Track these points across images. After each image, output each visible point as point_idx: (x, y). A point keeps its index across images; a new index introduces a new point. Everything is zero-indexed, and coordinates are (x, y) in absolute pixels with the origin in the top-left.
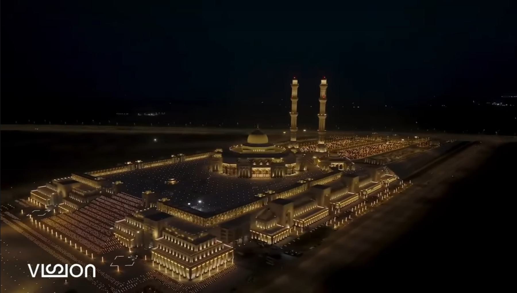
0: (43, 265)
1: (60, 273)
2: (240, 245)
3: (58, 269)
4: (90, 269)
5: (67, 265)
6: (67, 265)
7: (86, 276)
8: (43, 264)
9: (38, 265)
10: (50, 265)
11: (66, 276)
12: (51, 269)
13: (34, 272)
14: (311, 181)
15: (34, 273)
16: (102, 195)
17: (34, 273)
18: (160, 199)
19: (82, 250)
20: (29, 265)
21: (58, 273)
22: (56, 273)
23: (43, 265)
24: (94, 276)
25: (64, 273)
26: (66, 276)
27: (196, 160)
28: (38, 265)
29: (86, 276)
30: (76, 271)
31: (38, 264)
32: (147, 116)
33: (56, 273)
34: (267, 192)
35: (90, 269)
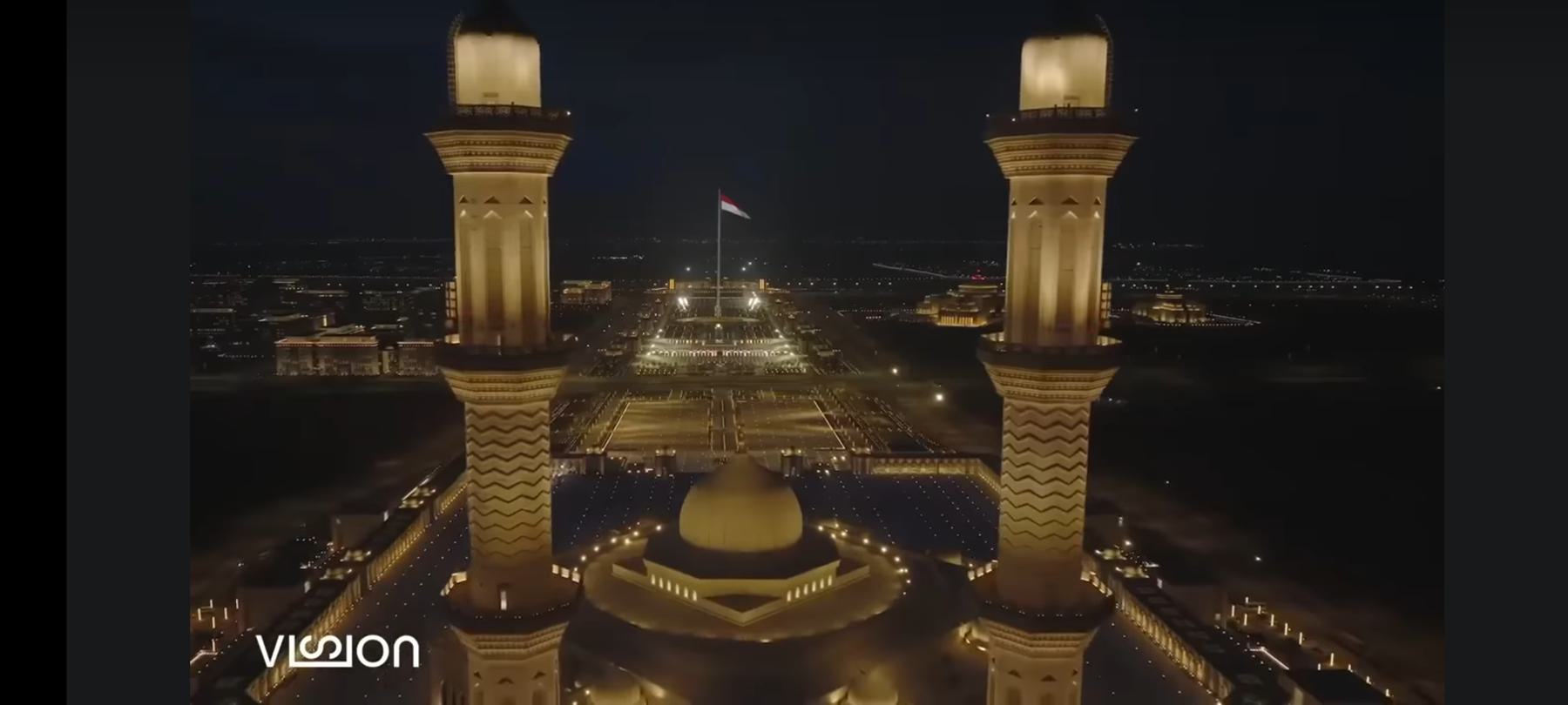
0: (292, 638)
1: (332, 656)
2: (1271, 667)
3: (330, 647)
4: (406, 647)
5: (349, 639)
6: (349, 639)
7: (397, 664)
8: (349, 634)
9: (281, 638)
10: (308, 639)
11: (348, 663)
12: (312, 648)
13: (270, 655)
14: (368, 560)
15: (270, 656)
16: (981, 459)
17: (270, 656)
18: (1100, 551)
19: (1335, 661)
20: (259, 638)
21: (329, 656)
22: (325, 657)
23: (292, 638)
24: (416, 664)
25: (342, 657)
26: (348, 663)
27: (907, 479)
28: (281, 638)
29: (397, 664)
30: (373, 651)
31: (282, 634)
32: (717, 196)
33: (325, 657)
34: (346, 559)
35: (406, 647)
